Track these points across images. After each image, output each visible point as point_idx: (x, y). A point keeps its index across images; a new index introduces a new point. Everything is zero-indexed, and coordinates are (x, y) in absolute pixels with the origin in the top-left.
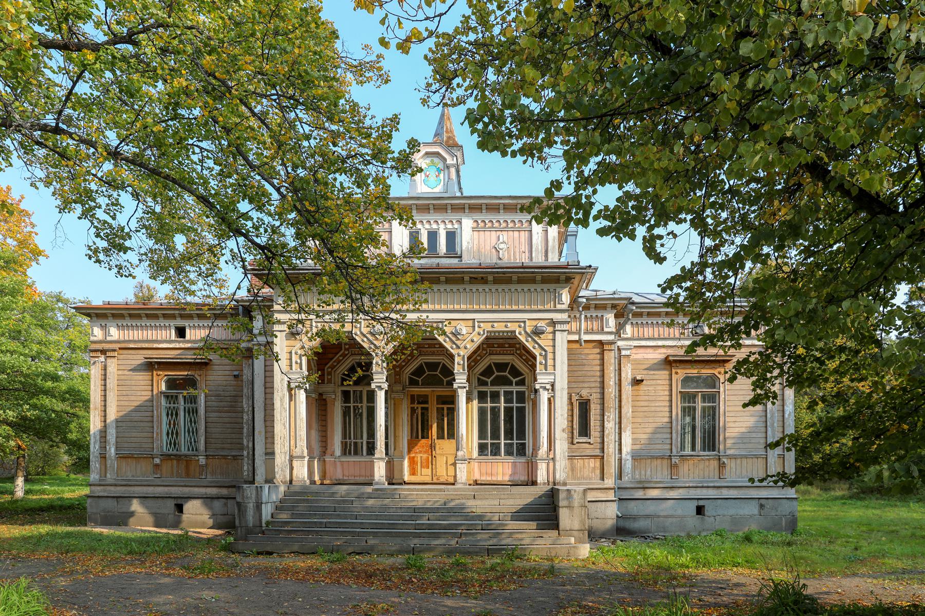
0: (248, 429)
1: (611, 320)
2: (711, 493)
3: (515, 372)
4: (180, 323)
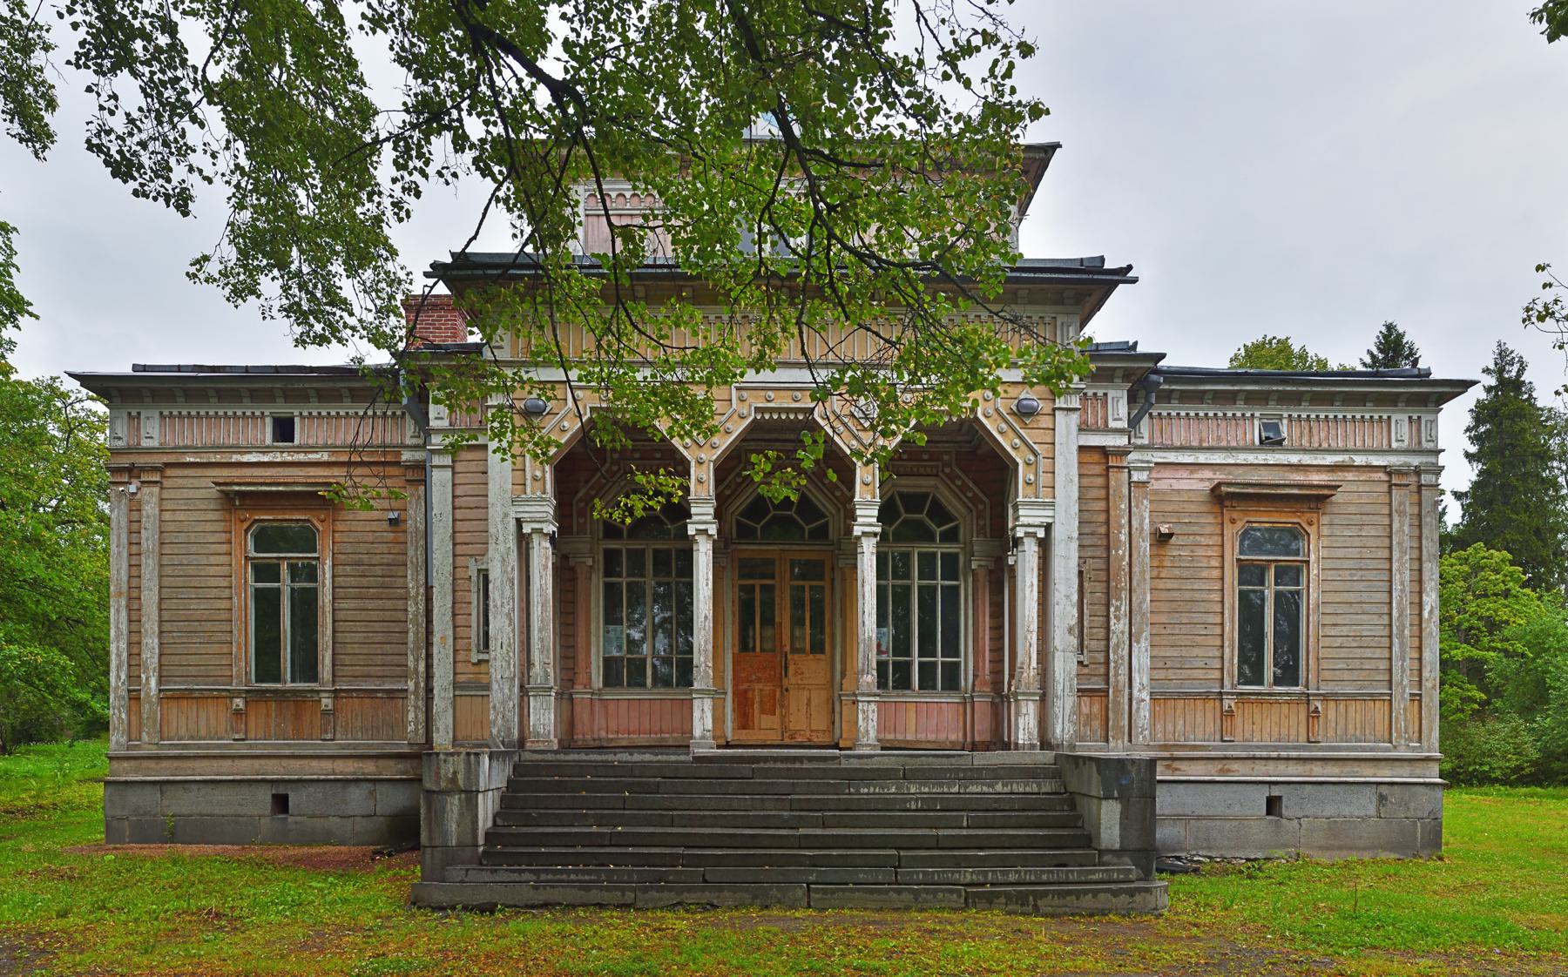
0: (416, 634)
2: (1293, 772)
4: (283, 410)
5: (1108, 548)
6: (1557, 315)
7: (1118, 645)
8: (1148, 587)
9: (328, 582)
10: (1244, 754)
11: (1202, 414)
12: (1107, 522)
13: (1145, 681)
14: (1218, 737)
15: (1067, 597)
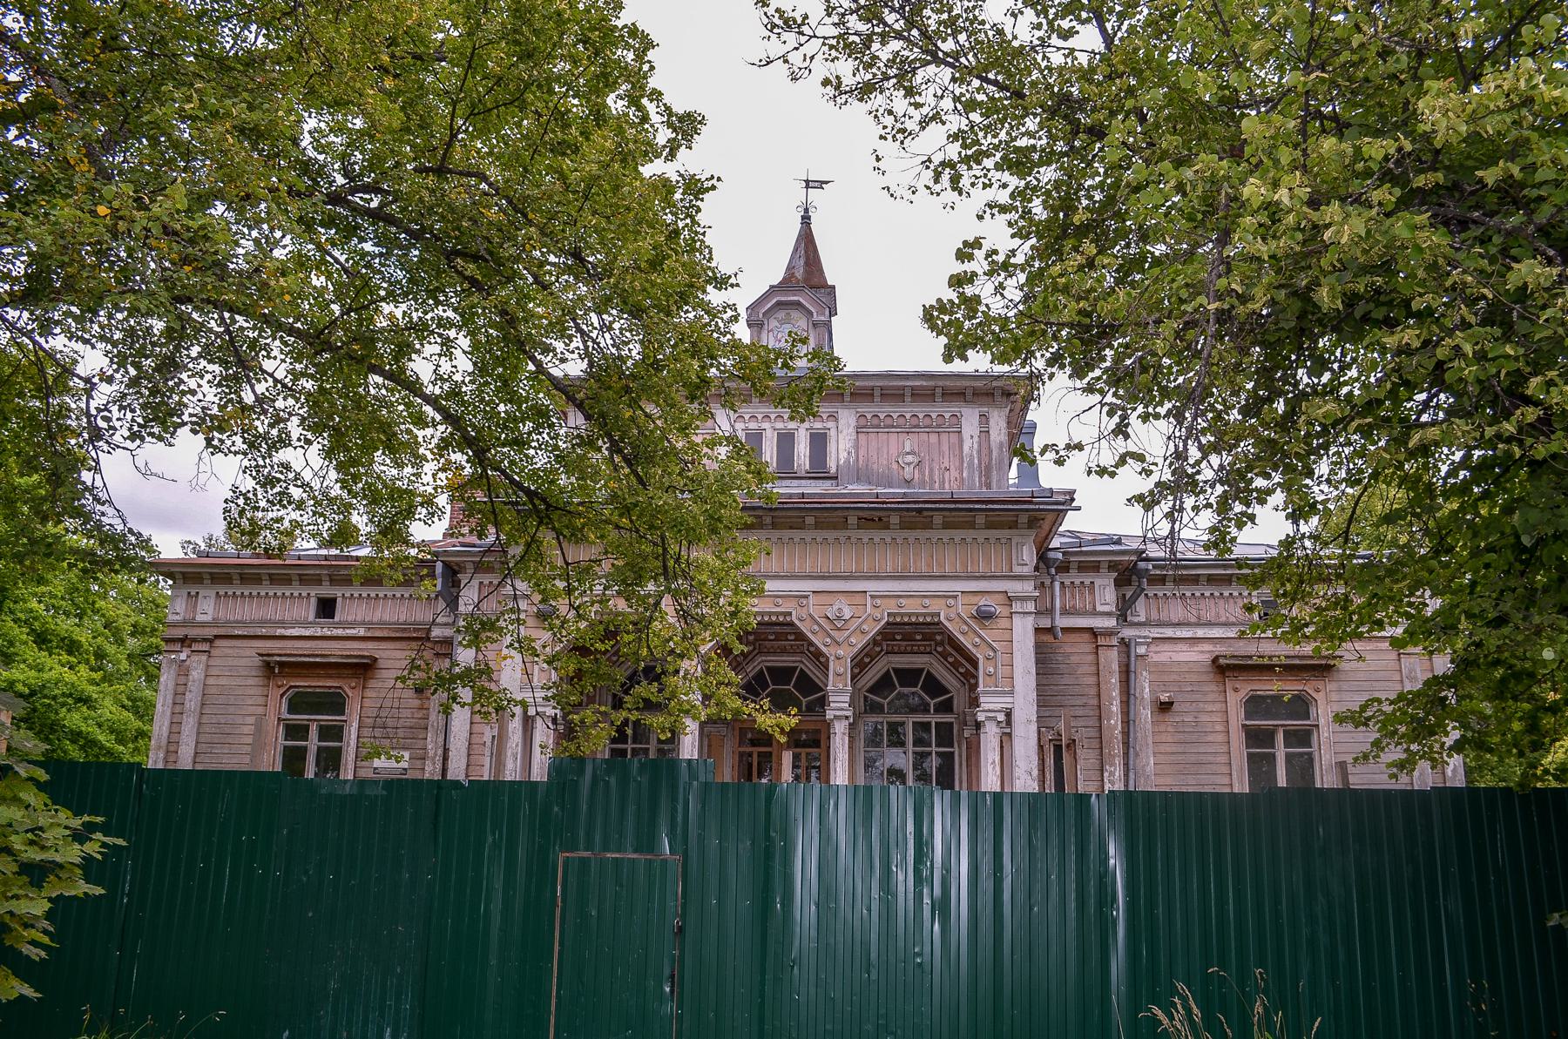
1: (1106, 594)
3: (934, 687)
4: (326, 591)
9: (353, 743)
11: (1198, 594)
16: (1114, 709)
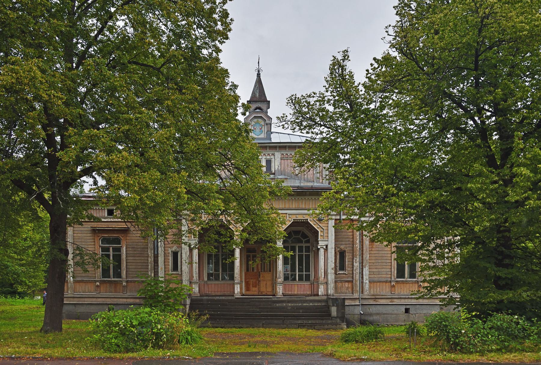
2: (414, 302)
5: (353, 245)
6: (362, 199)
7: (356, 269)
8: (368, 253)
9: (124, 253)
10: (398, 297)
12: (353, 238)
13: (367, 278)
14: (390, 292)
15: (332, 261)
16: (357, 242)
